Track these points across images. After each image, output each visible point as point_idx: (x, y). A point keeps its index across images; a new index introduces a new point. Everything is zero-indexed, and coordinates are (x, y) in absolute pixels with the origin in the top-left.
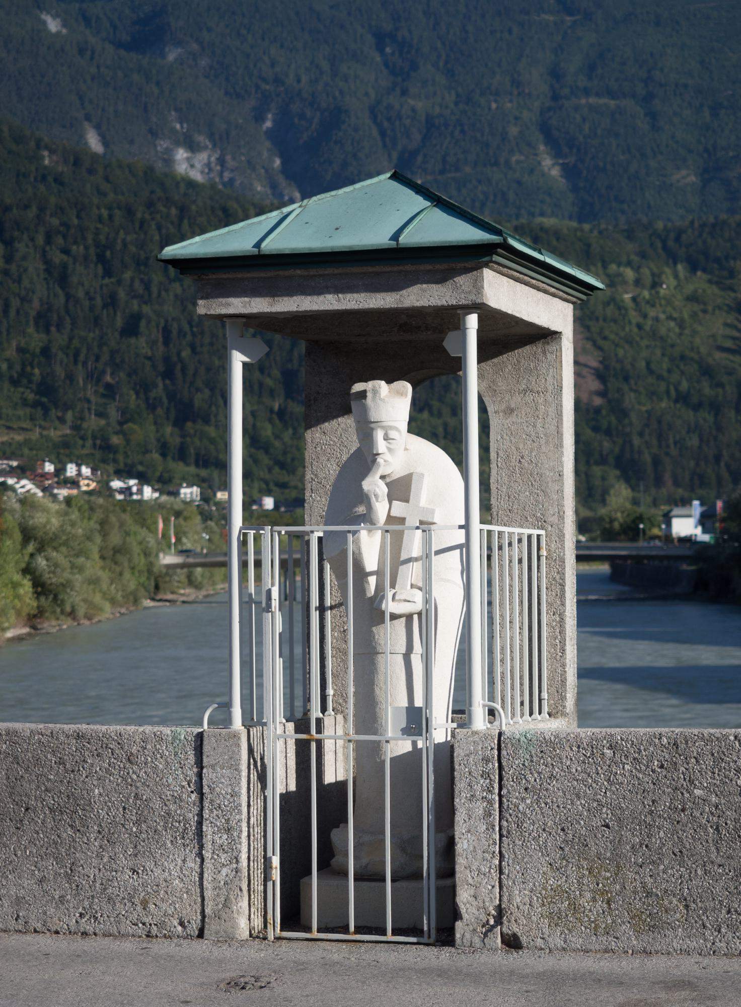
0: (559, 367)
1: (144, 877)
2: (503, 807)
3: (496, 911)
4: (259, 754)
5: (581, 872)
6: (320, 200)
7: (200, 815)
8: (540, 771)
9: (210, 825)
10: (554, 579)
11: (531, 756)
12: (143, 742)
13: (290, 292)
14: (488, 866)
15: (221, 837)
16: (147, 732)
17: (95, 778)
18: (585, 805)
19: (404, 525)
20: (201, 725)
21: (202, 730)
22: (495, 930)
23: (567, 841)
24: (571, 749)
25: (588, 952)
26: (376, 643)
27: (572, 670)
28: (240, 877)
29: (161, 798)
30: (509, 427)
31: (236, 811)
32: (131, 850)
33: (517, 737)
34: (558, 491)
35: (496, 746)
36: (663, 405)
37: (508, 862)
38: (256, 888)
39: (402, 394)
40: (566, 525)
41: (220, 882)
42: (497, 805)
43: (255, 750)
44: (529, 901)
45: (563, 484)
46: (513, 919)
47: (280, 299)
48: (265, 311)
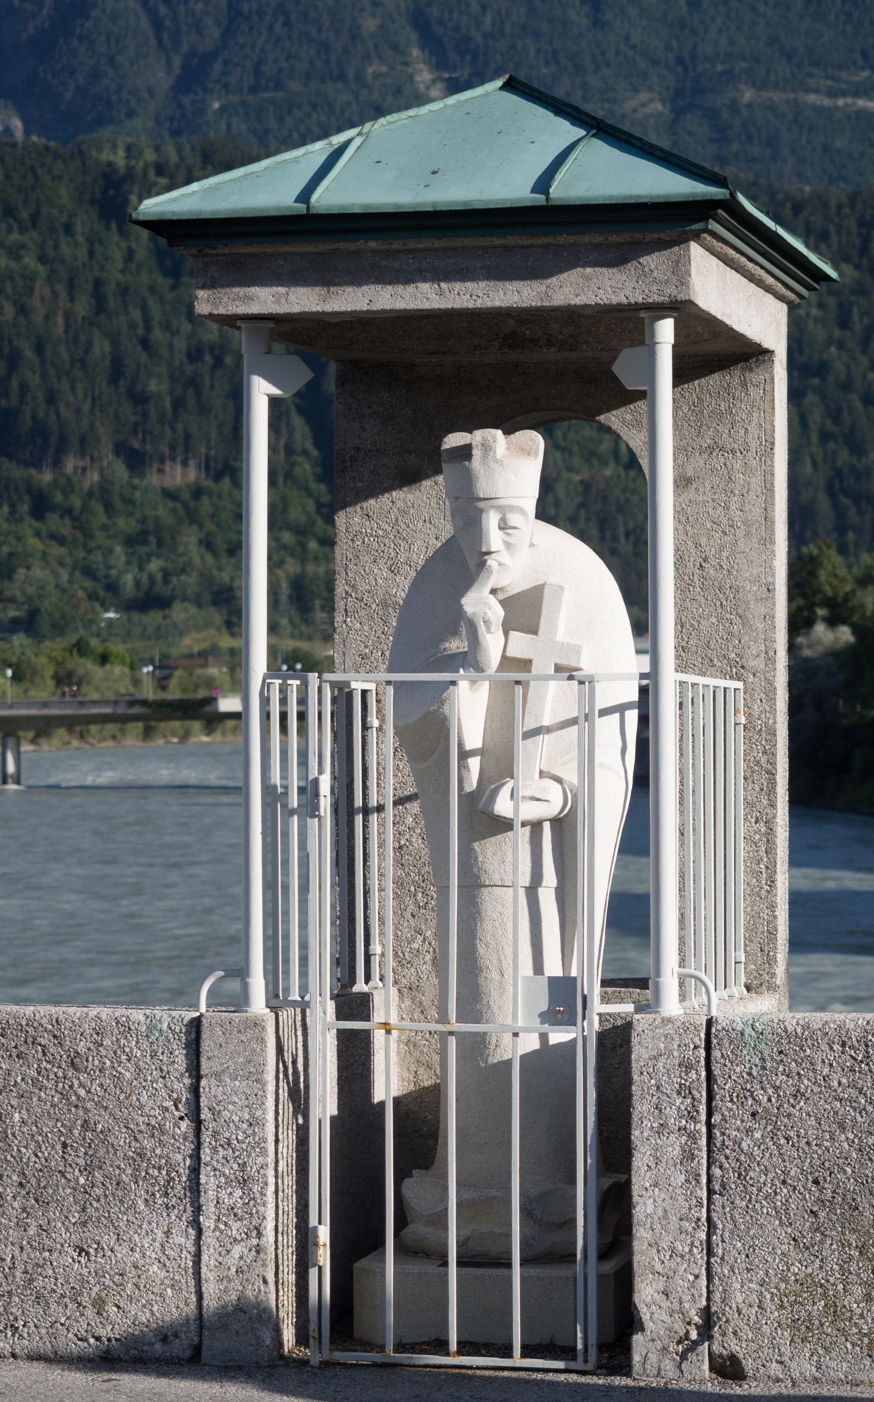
0: (768, 410)
1: (99, 1260)
2: (715, 1144)
3: (700, 1317)
4: (290, 1054)
5: (846, 1253)
6: (390, 123)
7: (196, 1156)
8: (778, 1084)
9: (212, 1173)
10: (758, 763)
11: (763, 1060)
12: (98, 1034)
13: (357, 279)
14: (689, 1241)
15: (231, 1194)
16: (104, 1017)
17: (14, 1094)
18: (853, 1142)
19: (530, 671)
20: (196, 1006)
21: (198, 1014)
22: (700, 1348)
23: (822, 1201)
24: (831, 1048)
25: (857, 1385)
26: (479, 869)
27: (783, 913)
28: (264, 1260)
29: (128, 1128)
30: (683, 509)
31: (258, 1150)
32: (76, 1214)
33: (738, 1028)
34: (765, 617)
35: (703, 1043)
36: (608, 472)
37: (722, 1236)
38: (285, 1280)
39: (529, 452)
40: (778, 674)
41: (229, 1268)
42: (703, 1142)
43: (286, 1048)
44: (757, 1301)
45: (774, 605)
46: (731, 1330)
47: (340, 290)
48: (314, 310)
